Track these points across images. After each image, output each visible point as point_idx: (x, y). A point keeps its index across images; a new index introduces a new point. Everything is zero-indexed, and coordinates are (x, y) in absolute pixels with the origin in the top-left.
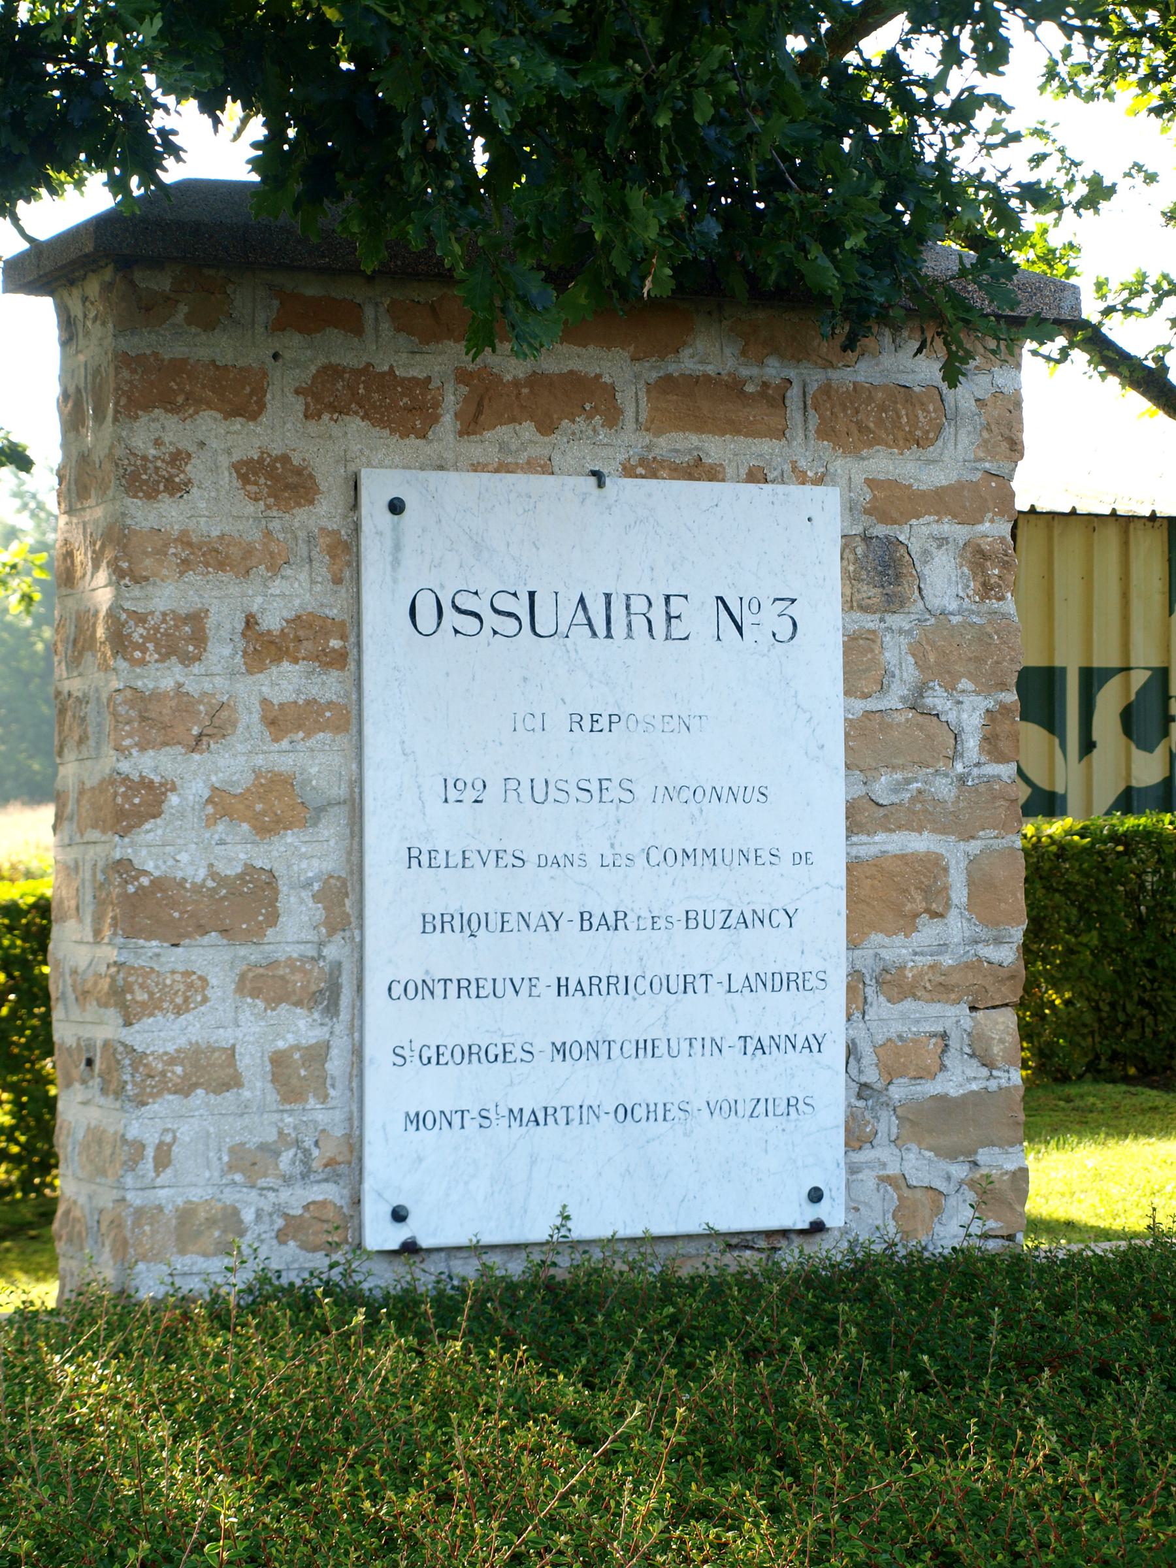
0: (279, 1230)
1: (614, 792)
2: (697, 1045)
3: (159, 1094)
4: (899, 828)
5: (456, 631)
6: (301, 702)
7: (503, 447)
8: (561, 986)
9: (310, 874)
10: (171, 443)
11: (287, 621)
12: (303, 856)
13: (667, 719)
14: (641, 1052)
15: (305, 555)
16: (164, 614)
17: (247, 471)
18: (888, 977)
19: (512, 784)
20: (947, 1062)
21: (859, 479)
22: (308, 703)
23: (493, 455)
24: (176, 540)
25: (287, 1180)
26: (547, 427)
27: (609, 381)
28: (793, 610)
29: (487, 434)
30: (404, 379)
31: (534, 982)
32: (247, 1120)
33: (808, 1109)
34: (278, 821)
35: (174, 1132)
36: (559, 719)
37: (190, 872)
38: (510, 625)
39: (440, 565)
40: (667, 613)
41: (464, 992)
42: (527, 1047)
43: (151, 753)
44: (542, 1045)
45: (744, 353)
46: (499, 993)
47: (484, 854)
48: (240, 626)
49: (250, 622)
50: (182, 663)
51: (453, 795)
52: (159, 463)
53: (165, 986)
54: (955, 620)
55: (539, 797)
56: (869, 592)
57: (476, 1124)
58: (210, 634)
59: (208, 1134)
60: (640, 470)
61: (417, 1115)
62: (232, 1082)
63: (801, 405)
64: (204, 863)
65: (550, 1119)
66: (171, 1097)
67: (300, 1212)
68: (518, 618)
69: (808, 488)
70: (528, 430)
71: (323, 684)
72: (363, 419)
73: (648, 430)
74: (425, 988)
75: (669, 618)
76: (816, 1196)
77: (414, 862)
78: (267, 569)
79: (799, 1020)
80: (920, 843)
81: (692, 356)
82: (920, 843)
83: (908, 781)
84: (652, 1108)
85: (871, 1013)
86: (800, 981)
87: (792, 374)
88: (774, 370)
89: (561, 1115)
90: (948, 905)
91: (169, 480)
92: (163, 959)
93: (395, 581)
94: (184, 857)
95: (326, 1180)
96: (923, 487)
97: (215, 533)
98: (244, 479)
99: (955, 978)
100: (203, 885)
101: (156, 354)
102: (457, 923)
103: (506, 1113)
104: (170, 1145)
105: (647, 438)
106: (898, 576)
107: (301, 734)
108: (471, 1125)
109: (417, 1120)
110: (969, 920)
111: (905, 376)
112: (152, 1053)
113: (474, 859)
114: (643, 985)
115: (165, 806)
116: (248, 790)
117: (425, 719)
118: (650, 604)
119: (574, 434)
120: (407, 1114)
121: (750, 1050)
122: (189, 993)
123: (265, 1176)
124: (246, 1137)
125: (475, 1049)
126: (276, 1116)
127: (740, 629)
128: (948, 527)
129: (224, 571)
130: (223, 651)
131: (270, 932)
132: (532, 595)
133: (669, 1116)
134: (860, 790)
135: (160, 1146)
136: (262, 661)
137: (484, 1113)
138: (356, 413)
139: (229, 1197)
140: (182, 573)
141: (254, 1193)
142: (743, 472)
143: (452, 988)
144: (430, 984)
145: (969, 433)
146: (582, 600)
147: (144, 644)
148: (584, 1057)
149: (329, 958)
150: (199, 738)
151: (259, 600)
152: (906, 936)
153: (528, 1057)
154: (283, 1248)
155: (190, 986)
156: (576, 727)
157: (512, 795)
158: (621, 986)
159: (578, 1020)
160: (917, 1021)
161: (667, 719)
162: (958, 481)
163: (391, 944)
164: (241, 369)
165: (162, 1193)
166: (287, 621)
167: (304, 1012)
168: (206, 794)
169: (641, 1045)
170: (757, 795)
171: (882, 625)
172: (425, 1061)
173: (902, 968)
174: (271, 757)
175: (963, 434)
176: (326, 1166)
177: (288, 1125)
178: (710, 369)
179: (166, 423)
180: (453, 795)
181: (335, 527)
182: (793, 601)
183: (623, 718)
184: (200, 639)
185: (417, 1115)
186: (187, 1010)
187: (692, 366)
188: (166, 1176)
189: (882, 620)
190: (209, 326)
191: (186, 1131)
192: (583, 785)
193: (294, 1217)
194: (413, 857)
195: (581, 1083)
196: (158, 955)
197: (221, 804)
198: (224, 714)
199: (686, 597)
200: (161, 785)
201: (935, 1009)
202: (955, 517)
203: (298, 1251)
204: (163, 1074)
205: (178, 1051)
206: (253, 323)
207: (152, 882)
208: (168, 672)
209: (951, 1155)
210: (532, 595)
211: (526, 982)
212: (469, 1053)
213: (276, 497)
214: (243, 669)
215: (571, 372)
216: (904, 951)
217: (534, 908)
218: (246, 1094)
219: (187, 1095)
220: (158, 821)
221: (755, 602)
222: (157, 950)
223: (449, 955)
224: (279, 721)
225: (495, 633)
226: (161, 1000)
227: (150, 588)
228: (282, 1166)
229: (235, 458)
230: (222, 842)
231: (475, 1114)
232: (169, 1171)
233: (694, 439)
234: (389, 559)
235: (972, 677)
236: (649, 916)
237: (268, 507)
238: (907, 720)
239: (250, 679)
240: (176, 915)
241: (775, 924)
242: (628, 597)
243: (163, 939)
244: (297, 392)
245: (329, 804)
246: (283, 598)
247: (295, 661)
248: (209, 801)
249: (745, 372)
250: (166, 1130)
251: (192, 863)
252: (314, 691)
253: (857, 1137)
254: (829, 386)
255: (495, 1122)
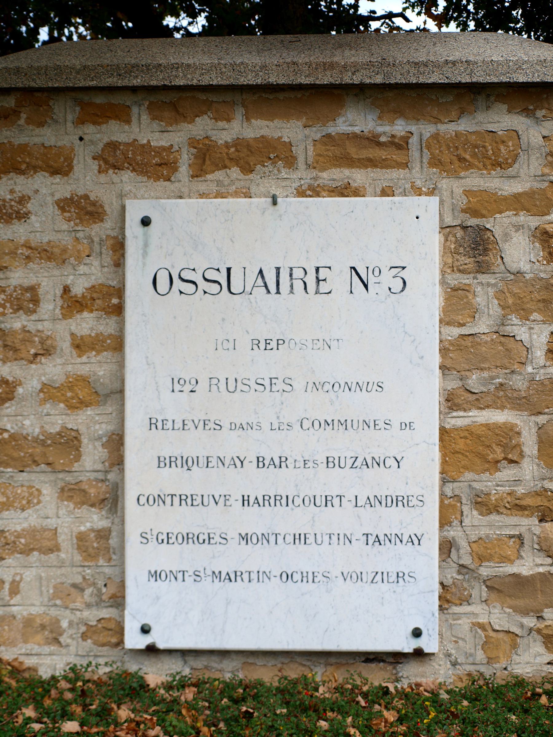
0: (83, 633)
1: (279, 385)
2: (335, 538)
3: (13, 553)
4: (488, 407)
5: (181, 292)
6: (93, 335)
7: (219, 183)
8: (245, 501)
9: (100, 432)
10: (19, 192)
11: (86, 289)
12: (97, 422)
13: (315, 342)
14: (297, 541)
15: (98, 251)
16: (15, 287)
17: (64, 205)
18: (479, 499)
19: (214, 381)
20: (523, 554)
21: (458, 191)
22: (97, 335)
23: (214, 188)
24: (22, 245)
25: (89, 606)
26: (248, 169)
27: (287, 140)
28: (403, 274)
29: (209, 177)
30: (156, 147)
31: (227, 497)
32: (63, 570)
33: (412, 580)
34: (81, 402)
35: (21, 575)
36: (244, 343)
37: (30, 431)
38: (215, 288)
39: (171, 254)
40: (317, 278)
41: (183, 502)
42: (223, 536)
43: (9, 364)
44: (233, 535)
45: (380, 118)
46: (206, 503)
47: (196, 422)
48: (59, 292)
49: (66, 290)
50: (25, 314)
51: (177, 387)
52: (13, 203)
53: (17, 494)
54: (528, 277)
55: (231, 389)
56: (469, 262)
57: (192, 579)
58: (41, 297)
59: (41, 578)
60: (309, 192)
61: (156, 572)
62: (56, 548)
63: (419, 147)
64: (38, 426)
65: (239, 579)
66: (19, 556)
67: (94, 623)
68: (219, 284)
69: (423, 198)
70: (235, 172)
71: (107, 324)
72: (132, 171)
73: (314, 168)
74: (160, 499)
75: (318, 280)
76: (417, 633)
77: (153, 426)
78: (75, 260)
79: (404, 525)
80: (499, 417)
81: (345, 122)
82: (499, 417)
83: (492, 378)
84: (305, 574)
85: (467, 522)
86: (405, 501)
87: (413, 129)
88: (399, 128)
89: (246, 576)
90: (522, 455)
91: (18, 212)
92: (15, 479)
93: (144, 264)
94: (27, 422)
95: (111, 606)
96: (505, 193)
97: (45, 240)
98: (63, 209)
99: (528, 501)
100: (37, 438)
101: (10, 142)
102: (179, 462)
103: (211, 574)
104: (19, 582)
105: (314, 173)
106: (486, 250)
107: (94, 353)
108: (189, 580)
109: (156, 575)
110: (538, 465)
111: (492, 125)
112: (8, 531)
113: (190, 425)
114: (298, 501)
115: (15, 394)
116: (62, 385)
117: (160, 343)
118: (306, 273)
119: (265, 173)
120: (150, 572)
121: (371, 542)
122: (31, 500)
123: (74, 602)
124: (64, 579)
125: (190, 536)
126: (80, 569)
127: (366, 286)
128: (523, 218)
129: (50, 261)
130: (49, 306)
131: (76, 464)
132: (229, 270)
133: (316, 580)
134: (453, 384)
135: (14, 581)
136: (72, 312)
137: (197, 573)
138: (128, 168)
139: (53, 612)
140: (26, 264)
141: (68, 612)
142: (378, 191)
143: (176, 500)
144: (163, 497)
145: (538, 158)
146: (261, 272)
147: (4, 304)
148: (260, 543)
149: (111, 481)
150: (36, 355)
151: (71, 277)
152: (490, 474)
153: (224, 541)
154: (84, 643)
155: (31, 494)
156: (255, 347)
157: (214, 388)
158: (284, 501)
159: (256, 520)
160: (500, 527)
161: (315, 342)
162: (531, 188)
163: (140, 474)
164: (60, 147)
165: (14, 609)
166: (86, 289)
167: (97, 511)
168: (39, 387)
169: (297, 537)
170: (376, 387)
171: (475, 281)
172: (160, 541)
173: (488, 494)
174: (76, 366)
175: (533, 158)
176: (110, 598)
177: (88, 574)
178: (357, 130)
179: (17, 180)
180: (177, 387)
181: (115, 234)
182: (404, 268)
183: (286, 342)
184: (36, 301)
185: (156, 572)
186: (29, 508)
187: (345, 128)
188: (16, 599)
189: (475, 278)
190: (41, 124)
191: (29, 575)
192: (259, 381)
193: (92, 626)
194: (152, 424)
195: (256, 558)
196: (12, 477)
197: (49, 392)
198: (49, 342)
199: (330, 268)
200: (13, 382)
201: (513, 520)
202: (528, 211)
203: (92, 646)
204: (14, 542)
205: (23, 530)
206: (66, 121)
207: (10, 436)
208: (18, 320)
209: (525, 612)
210: (229, 270)
211: (223, 497)
212: (187, 538)
213: (81, 219)
214: (60, 317)
215: (262, 137)
216: (490, 483)
217: (228, 454)
218: (63, 555)
219: (28, 555)
220: (13, 402)
221: (377, 270)
222: (11, 474)
223: (173, 480)
224: (80, 345)
225: (205, 292)
226: (14, 502)
227: (8, 273)
228: (85, 597)
229: (58, 196)
230: (48, 415)
231: (191, 573)
232: (18, 596)
233: (347, 172)
234: (142, 251)
235: (539, 311)
236: (302, 460)
237: (76, 225)
238: (492, 340)
239: (65, 322)
240: (22, 454)
241: (387, 466)
242: (291, 269)
243: (14, 467)
244: (94, 158)
245: (111, 393)
246: (85, 276)
247: (92, 311)
248: (41, 391)
249: (380, 129)
250: (17, 574)
251: (32, 425)
252: (101, 328)
253: (448, 597)
254: (438, 134)
255: (203, 579)
